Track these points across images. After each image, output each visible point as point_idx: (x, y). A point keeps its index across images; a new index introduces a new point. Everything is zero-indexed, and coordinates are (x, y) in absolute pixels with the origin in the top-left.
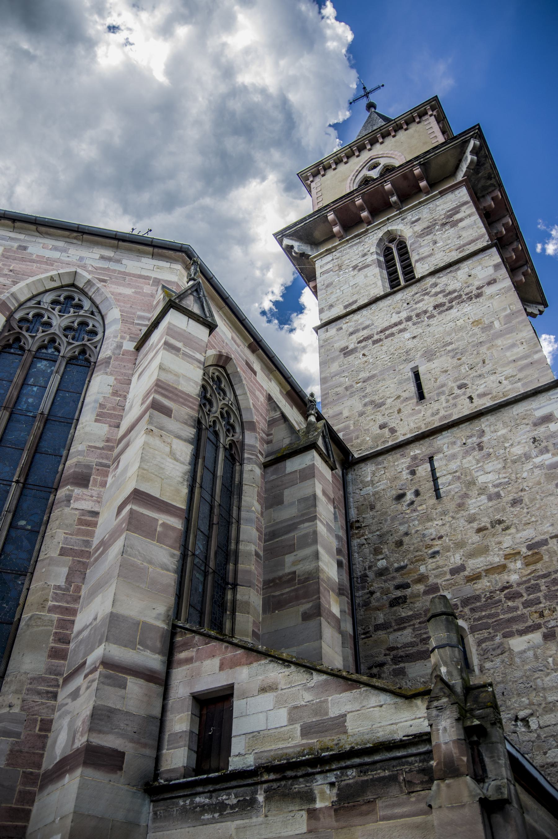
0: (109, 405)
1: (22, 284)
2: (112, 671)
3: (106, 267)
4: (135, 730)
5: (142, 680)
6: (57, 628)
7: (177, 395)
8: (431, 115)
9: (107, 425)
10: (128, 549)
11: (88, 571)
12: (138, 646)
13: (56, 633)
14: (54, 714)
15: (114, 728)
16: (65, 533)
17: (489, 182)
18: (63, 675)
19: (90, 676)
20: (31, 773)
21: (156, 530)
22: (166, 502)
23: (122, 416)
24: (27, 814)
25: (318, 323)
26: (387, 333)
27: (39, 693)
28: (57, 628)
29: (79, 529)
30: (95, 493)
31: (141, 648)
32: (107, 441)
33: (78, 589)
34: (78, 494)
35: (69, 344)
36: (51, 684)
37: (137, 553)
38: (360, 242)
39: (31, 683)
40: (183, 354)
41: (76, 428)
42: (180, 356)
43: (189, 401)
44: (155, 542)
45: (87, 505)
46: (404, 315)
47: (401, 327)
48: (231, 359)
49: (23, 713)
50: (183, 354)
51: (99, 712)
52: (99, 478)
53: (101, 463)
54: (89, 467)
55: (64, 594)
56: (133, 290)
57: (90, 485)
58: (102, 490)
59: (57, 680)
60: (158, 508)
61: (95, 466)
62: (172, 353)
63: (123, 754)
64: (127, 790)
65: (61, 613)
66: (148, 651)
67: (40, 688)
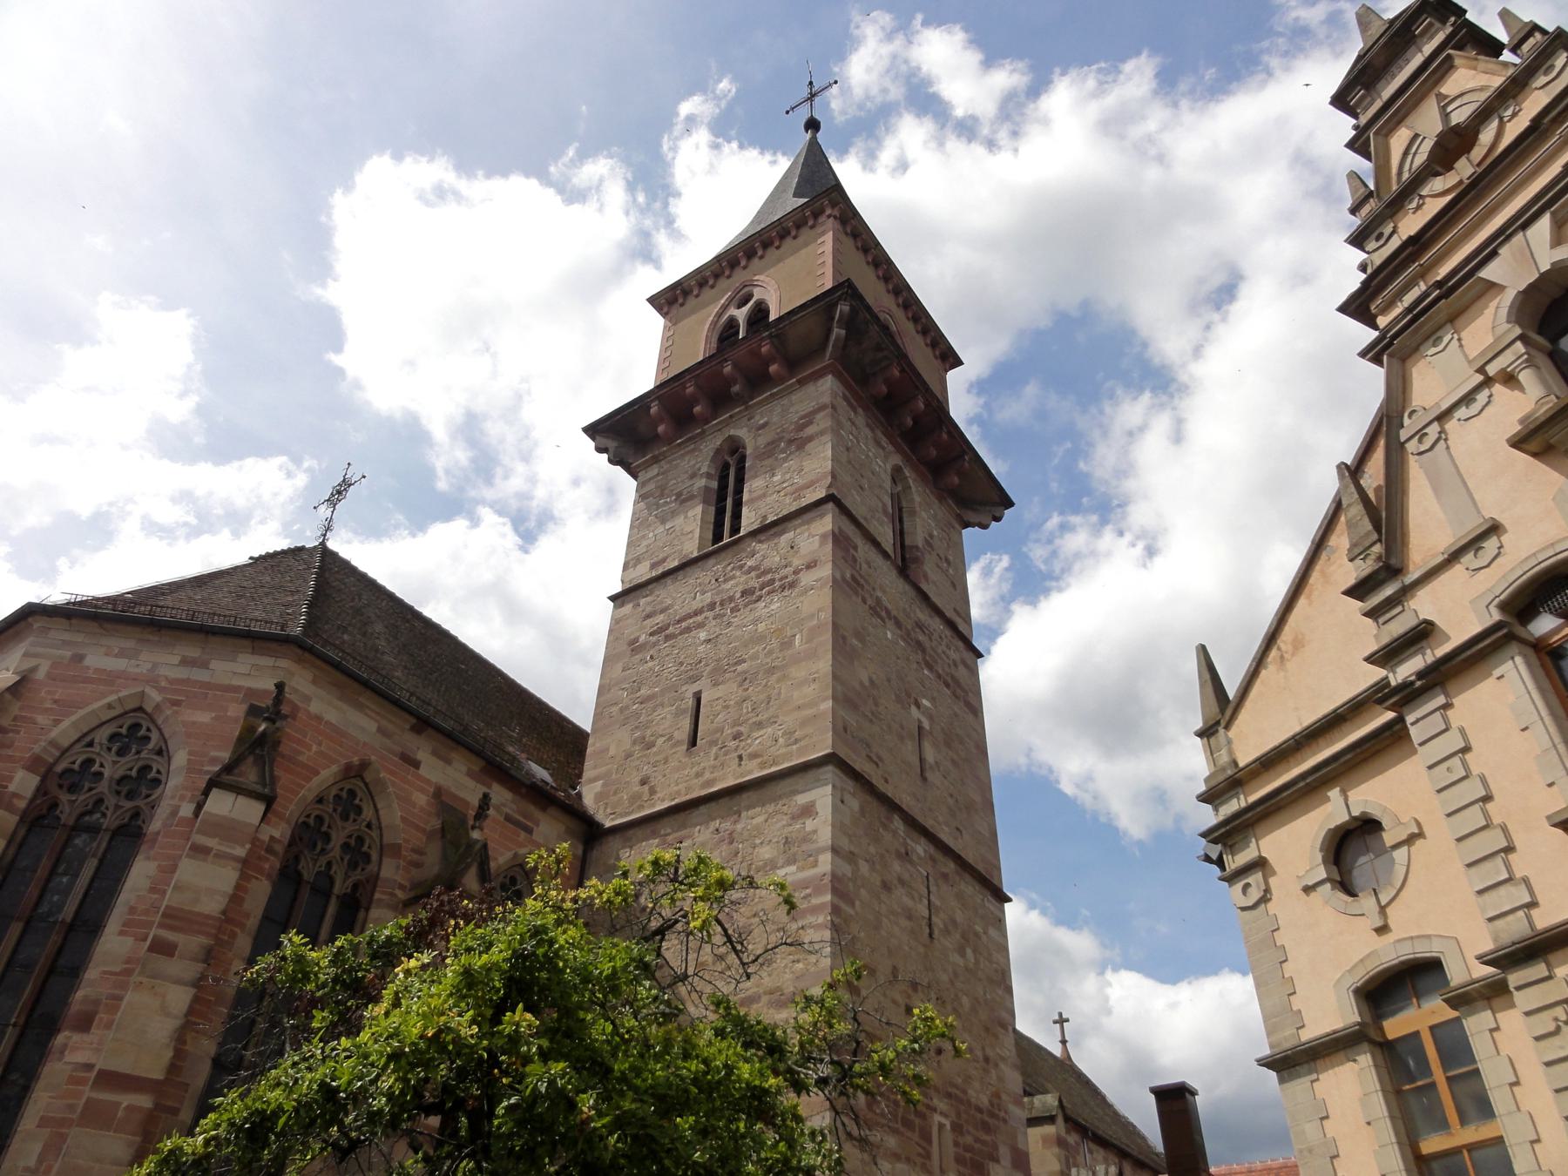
1: (66, 723)
3: (185, 677)
8: (829, 216)
17: (880, 355)
25: (618, 588)
26: (684, 624)
32: (127, 962)
38: (693, 450)
44: (111, 1133)
46: (708, 598)
47: (699, 618)
48: (370, 764)
56: (213, 715)
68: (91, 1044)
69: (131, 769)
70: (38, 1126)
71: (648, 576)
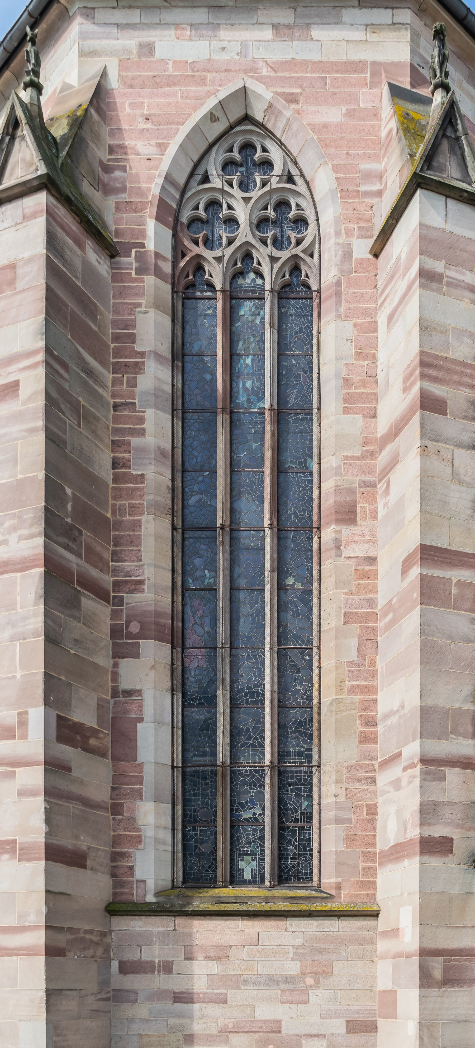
0: (356, 378)
2: (431, 766)
3: (289, 57)
4: (459, 817)
5: (459, 769)
6: (361, 710)
7: (448, 370)
9: (361, 416)
10: (425, 628)
11: (379, 638)
12: (451, 736)
13: (361, 716)
14: (377, 798)
15: (440, 818)
16: (344, 594)
18: (377, 759)
19: (409, 771)
20: (369, 852)
21: (450, 593)
22: (458, 552)
23: (376, 394)
24: (373, 885)
27: (359, 780)
28: (361, 710)
29: (358, 585)
30: (366, 531)
31: (454, 737)
32: (366, 443)
33: (373, 662)
34: (347, 536)
35: (274, 259)
36: (368, 770)
37: (435, 629)
39: (348, 772)
40: (448, 284)
41: (320, 424)
42: (445, 289)
43: (467, 375)
44: (452, 611)
45: (360, 550)
49: (348, 800)
50: (448, 284)
51: (425, 807)
52: (367, 505)
53: (364, 482)
54: (351, 491)
55: (359, 671)
57: (358, 519)
58: (373, 523)
59: (373, 765)
60: (449, 563)
61: (358, 489)
62: (432, 290)
63: (452, 839)
64: (459, 869)
65: (362, 693)
66: (461, 738)
67: (358, 775)
68: (364, 536)
69: (266, 208)
70: (345, 623)
71: (389, 475)
